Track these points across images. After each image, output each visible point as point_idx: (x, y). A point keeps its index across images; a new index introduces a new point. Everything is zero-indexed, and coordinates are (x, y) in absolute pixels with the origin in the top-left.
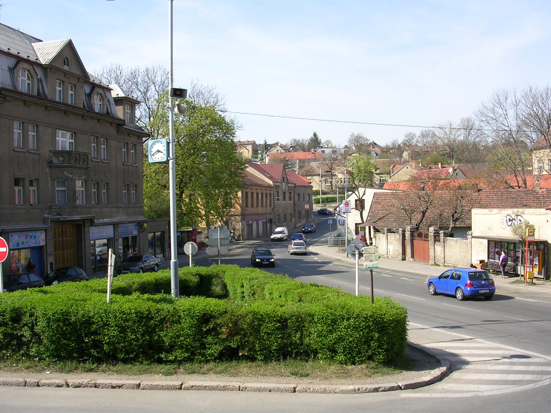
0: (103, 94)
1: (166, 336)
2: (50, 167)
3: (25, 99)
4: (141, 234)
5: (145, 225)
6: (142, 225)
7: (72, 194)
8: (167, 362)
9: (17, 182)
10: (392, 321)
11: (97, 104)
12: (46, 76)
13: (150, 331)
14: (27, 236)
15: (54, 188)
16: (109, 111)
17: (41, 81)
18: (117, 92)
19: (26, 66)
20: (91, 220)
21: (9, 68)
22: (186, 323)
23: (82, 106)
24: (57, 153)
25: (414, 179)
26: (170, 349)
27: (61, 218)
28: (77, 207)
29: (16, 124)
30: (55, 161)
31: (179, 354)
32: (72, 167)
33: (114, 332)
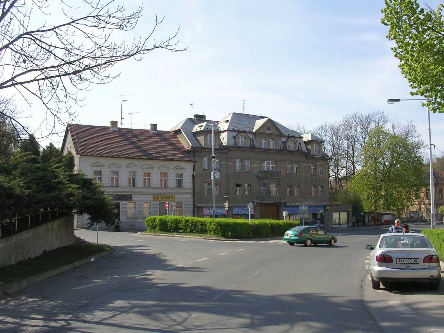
0: (295, 141)
1: (180, 226)
2: (258, 178)
3: (243, 149)
4: (326, 213)
5: (328, 207)
6: (326, 208)
7: (269, 191)
8: (180, 233)
9: (238, 186)
10: (224, 224)
11: (291, 146)
12: (255, 137)
13: (177, 224)
14: (243, 209)
15: (260, 188)
16: (300, 149)
17: (253, 140)
18: (307, 137)
19: (243, 134)
20: (285, 203)
21: (234, 137)
22: (184, 222)
23: (279, 149)
24: (262, 172)
25: (276, 186)
26: (181, 230)
27: (263, 202)
28: (271, 197)
29: (237, 161)
30: (261, 175)
31: (182, 231)
32: (268, 178)
33: (170, 224)
